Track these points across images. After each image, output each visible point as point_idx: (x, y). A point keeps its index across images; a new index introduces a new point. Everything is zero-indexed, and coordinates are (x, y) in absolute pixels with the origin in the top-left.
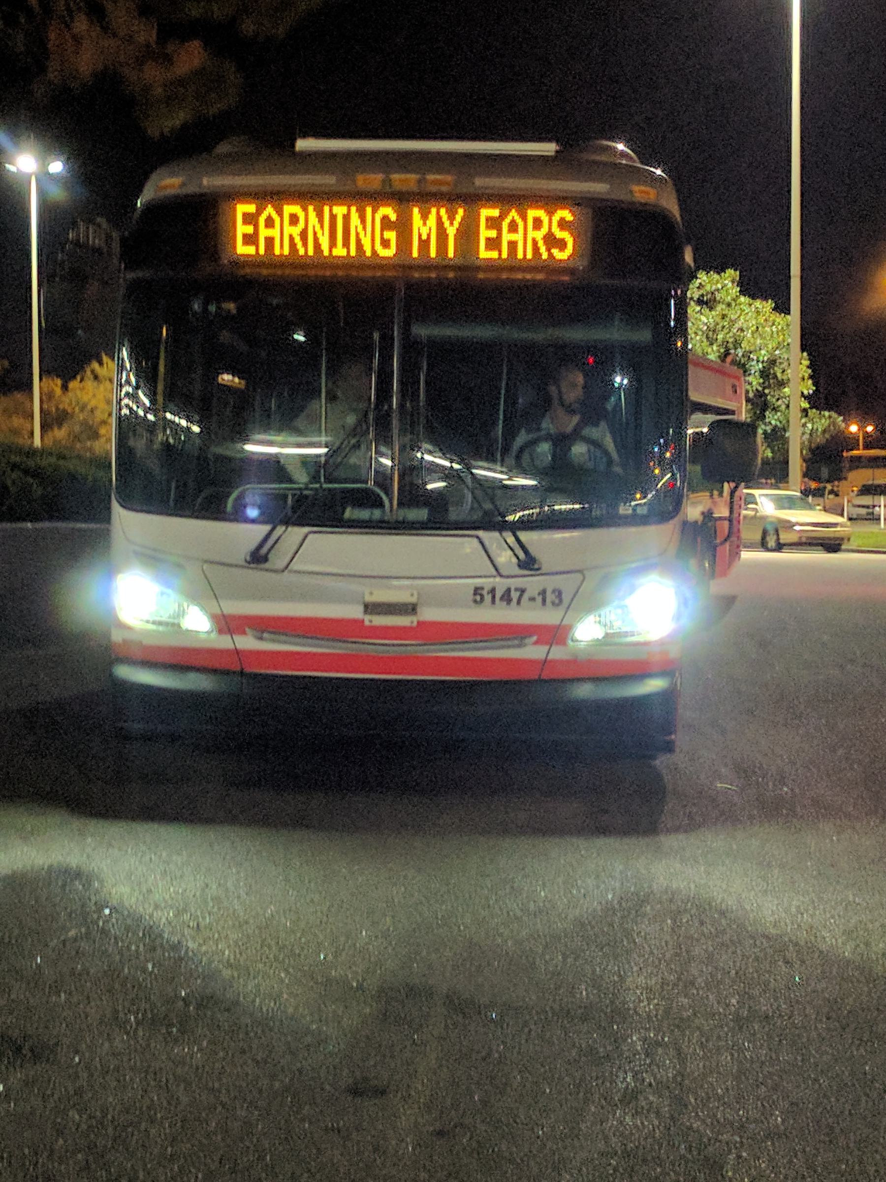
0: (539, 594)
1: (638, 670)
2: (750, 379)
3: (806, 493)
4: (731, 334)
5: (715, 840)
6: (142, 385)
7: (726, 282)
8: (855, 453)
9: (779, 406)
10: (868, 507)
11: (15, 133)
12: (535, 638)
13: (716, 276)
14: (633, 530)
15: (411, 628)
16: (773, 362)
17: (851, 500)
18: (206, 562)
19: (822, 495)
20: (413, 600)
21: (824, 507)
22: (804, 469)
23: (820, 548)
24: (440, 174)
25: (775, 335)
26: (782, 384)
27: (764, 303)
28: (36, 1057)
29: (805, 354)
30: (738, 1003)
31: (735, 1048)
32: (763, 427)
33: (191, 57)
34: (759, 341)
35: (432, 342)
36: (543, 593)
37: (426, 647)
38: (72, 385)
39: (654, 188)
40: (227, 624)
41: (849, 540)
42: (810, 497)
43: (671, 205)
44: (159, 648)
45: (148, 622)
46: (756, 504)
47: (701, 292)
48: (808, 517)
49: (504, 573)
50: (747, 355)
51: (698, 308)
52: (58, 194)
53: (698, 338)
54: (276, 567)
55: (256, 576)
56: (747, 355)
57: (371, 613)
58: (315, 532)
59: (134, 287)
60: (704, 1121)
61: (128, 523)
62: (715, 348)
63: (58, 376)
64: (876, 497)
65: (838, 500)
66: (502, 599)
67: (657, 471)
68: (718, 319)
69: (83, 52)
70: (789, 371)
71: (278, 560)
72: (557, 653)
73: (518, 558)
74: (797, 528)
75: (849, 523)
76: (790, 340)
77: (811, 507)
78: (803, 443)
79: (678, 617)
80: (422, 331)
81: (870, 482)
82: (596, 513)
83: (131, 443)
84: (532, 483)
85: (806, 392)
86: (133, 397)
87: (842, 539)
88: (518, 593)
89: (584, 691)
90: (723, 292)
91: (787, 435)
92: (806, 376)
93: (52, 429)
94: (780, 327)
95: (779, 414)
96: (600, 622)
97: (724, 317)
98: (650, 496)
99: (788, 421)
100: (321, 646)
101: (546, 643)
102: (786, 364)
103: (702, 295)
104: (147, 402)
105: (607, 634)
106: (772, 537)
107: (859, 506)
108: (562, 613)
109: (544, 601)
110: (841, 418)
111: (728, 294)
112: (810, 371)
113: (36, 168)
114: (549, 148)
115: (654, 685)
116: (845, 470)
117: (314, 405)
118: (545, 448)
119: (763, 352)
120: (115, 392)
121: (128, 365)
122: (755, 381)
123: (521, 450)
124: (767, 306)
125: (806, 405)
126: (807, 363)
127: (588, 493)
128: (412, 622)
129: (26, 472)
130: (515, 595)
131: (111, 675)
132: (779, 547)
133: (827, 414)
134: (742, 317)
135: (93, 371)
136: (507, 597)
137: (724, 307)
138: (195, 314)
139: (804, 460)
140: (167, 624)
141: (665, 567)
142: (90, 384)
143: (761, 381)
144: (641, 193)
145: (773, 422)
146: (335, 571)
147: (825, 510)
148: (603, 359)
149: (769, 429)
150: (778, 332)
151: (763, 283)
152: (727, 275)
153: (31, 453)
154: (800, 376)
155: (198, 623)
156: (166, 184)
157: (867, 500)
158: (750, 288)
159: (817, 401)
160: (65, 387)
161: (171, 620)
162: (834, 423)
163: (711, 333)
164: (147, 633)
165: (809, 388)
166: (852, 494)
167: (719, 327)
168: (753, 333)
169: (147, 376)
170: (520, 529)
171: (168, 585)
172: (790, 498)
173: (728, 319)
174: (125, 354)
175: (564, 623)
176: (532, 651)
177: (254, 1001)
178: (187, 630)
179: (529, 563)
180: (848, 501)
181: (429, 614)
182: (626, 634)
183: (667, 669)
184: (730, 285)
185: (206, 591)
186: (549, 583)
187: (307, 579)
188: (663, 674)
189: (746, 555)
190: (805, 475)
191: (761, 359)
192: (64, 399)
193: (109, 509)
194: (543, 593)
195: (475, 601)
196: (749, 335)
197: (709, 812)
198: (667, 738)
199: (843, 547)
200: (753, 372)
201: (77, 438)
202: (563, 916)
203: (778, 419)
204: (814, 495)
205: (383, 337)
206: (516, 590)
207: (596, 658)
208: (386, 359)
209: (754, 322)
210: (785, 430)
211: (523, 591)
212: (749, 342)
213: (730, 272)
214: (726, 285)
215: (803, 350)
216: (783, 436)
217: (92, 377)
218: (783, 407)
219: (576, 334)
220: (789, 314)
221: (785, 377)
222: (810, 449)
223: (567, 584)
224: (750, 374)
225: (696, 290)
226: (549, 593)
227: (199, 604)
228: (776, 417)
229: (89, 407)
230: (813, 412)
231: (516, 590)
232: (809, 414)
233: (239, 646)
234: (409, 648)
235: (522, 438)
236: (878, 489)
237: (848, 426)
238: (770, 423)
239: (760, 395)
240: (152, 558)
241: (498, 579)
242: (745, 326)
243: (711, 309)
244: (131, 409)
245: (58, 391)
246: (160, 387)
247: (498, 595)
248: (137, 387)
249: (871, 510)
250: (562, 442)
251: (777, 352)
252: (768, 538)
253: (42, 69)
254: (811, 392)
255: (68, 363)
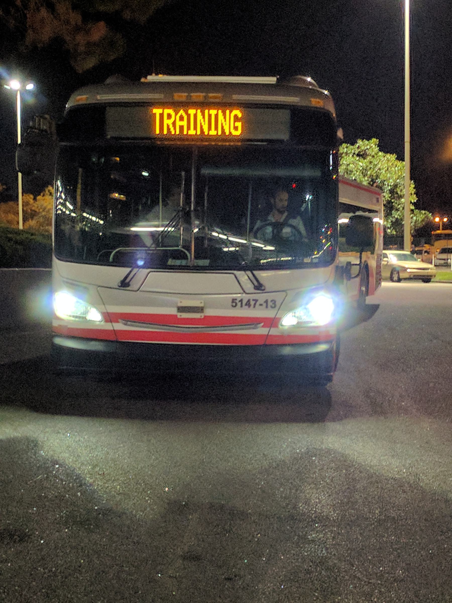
0: (265, 302)
1: (314, 340)
2: (384, 194)
3: (413, 252)
4: (374, 171)
5: (350, 425)
6: (68, 198)
7: (372, 145)
8: (438, 232)
9: (399, 208)
10: (444, 259)
11: (9, 69)
12: (262, 324)
13: (367, 142)
14: (314, 270)
15: (200, 319)
16: (396, 186)
17: (436, 256)
18: (99, 286)
19: (421, 254)
20: (202, 305)
21: (422, 260)
22: (412, 240)
23: (421, 280)
24: (216, 93)
25: (397, 172)
26: (400, 197)
27: (392, 155)
28: (21, 540)
29: (412, 182)
30: (379, 512)
31: (378, 536)
32: (391, 218)
33: (99, 31)
34: (389, 175)
35: (213, 178)
36: (266, 302)
37: (208, 329)
38: (39, 198)
39: (323, 100)
40: (109, 317)
41: (435, 276)
42: (415, 255)
43: (331, 108)
44: (77, 329)
45: (70, 316)
46: (387, 257)
47: (359, 150)
48: (414, 265)
49: (247, 292)
50: (383, 182)
51: (358, 158)
52: (31, 100)
53: (358, 173)
54: (133, 289)
55: (122, 293)
56: (383, 182)
57: (181, 312)
58: (153, 272)
59: (64, 150)
60: (362, 574)
61: (61, 267)
62: (366, 178)
63: (31, 193)
64: (449, 255)
65: (429, 256)
66: (246, 305)
67: (324, 241)
68: (368, 164)
69: (45, 27)
70: (404, 190)
71: (134, 285)
72: (273, 332)
73: (254, 284)
74: (409, 270)
75: (435, 268)
76: (404, 175)
77: (416, 260)
78: (411, 227)
79: (334, 315)
80: (206, 171)
81: (446, 247)
82: (298, 261)
83: (63, 227)
84: (273, 248)
85: (413, 202)
86: (64, 205)
87: (431, 276)
88: (254, 302)
89: (287, 351)
90: (371, 150)
91: (403, 223)
92: (413, 192)
93: (28, 221)
94: (399, 168)
95: (399, 212)
96: (295, 316)
97: (371, 162)
98: (320, 253)
99: (403, 216)
100: (148, 327)
101: (268, 327)
102: (402, 187)
103: (360, 152)
104: (71, 207)
105: (298, 323)
106: (396, 275)
107: (440, 259)
108: (276, 311)
109: (267, 307)
110: (431, 214)
111: (373, 151)
112: (415, 190)
113: (20, 87)
114: (272, 80)
115: (322, 347)
116: (432, 241)
117: (157, 208)
118: (269, 229)
119: (391, 181)
120: (56, 201)
121: (60, 189)
122: (387, 195)
123: (258, 229)
124: (392, 157)
125: (413, 207)
126: (413, 186)
127: (294, 252)
128: (201, 316)
129: (16, 242)
130: (252, 303)
131: (53, 343)
132: (399, 280)
133: (423, 212)
134: (380, 163)
135: (49, 191)
136: (248, 304)
137: (371, 157)
138: (93, 163)
139: (412, 236)
140: (79, 317)
141: (327, 288)
142: (47, 197)
143: (390, 195)
144: (315, 102)
145: (396, 216)
146: (172, 291)
147: (422, 261)
148: (302, 185)
149: (394, 220)
150: (398, 170)
151: (390, 145)
152: (372, 141)
153: (18, 232)
154: (410, 193)
155: (95, 316)
156: (79, 98)
157: (444, 256)
158: (384, 148)
159: (417, 205)
160: (35, 199)
161: (82, 315)
162: (427, 217)
163: (364, 171)
164: (69, 321)
165: (414, 199)
166: (437, 253)
167: (368, 168)
168: (385, 171)
169: (71, 194)
170: (254, 270)
171: (80, 298)
172: (404, 255)
173: (373, 164)
174: (59, 183)
175: (277, 317)
176: (261, 331)
177: (132, 512)
178: (90, 320)
179: (259, 287)
180: (434, 257)
181: (209, 312)
182: (308, 322)
183: (328, 339)
184: (374, 146)
185: (99, 301)
186: (269, 297)
187: (148, 295)
188: (326, 342)
189: (385, 284)
190: (412, 243)
191: (390, 184)
192: (34, 204)
193: (51, 261)
194: (266, 302)
195: (233, 306)
196: (384, 172)
197: (349, 411)
198: (329, 374)
199: (432, 280)
200: (386, 191)
201: (41, 225)
202: (290, 468)
203: (399, 215)
204: (417, 254)
205: (186, 176)
206: (253, 300)
207: (292, 334)
208: (188, 185)
209: (386, 165)
210: (402, 220)
211: (256, 301)
212: (384, 175)
213: (374, 140)
214: (372, 147)
215: (411, 179)
216: (401, 224)
217: (49, 193)
218: (401, 209)
219: (281, 172)
220: (404, 161)
221: (402, 194)
222: (415, 230)
223: (278, 297)
224: (384, 192)
225: (356, 149)
226: (269, 301)
227: (95, 307)
228: (397, 214)
229: (47, 209)
230: (416, 211)
231: (253, 300)
232: (415, 212)
233: (115, 329)
234: (199, 329)
235: (259, 224)
236: (450, 251)
237: (434, 219)
238: (394, 217)
239: (389, 202)
240: (73, 284)
241: (244, 295)
242: (382, 167)
243: (364, 159)
244: (61, 210)
245: (32, 201)
246: (79, 198)
247: (244, 302)
248: (65, 200)
249: (446, 261)
250: (278, 226)
251: (398, 181)
252: (394, 275)
253: (23, 36)
254: (415, 201)
255: (36, 187)
